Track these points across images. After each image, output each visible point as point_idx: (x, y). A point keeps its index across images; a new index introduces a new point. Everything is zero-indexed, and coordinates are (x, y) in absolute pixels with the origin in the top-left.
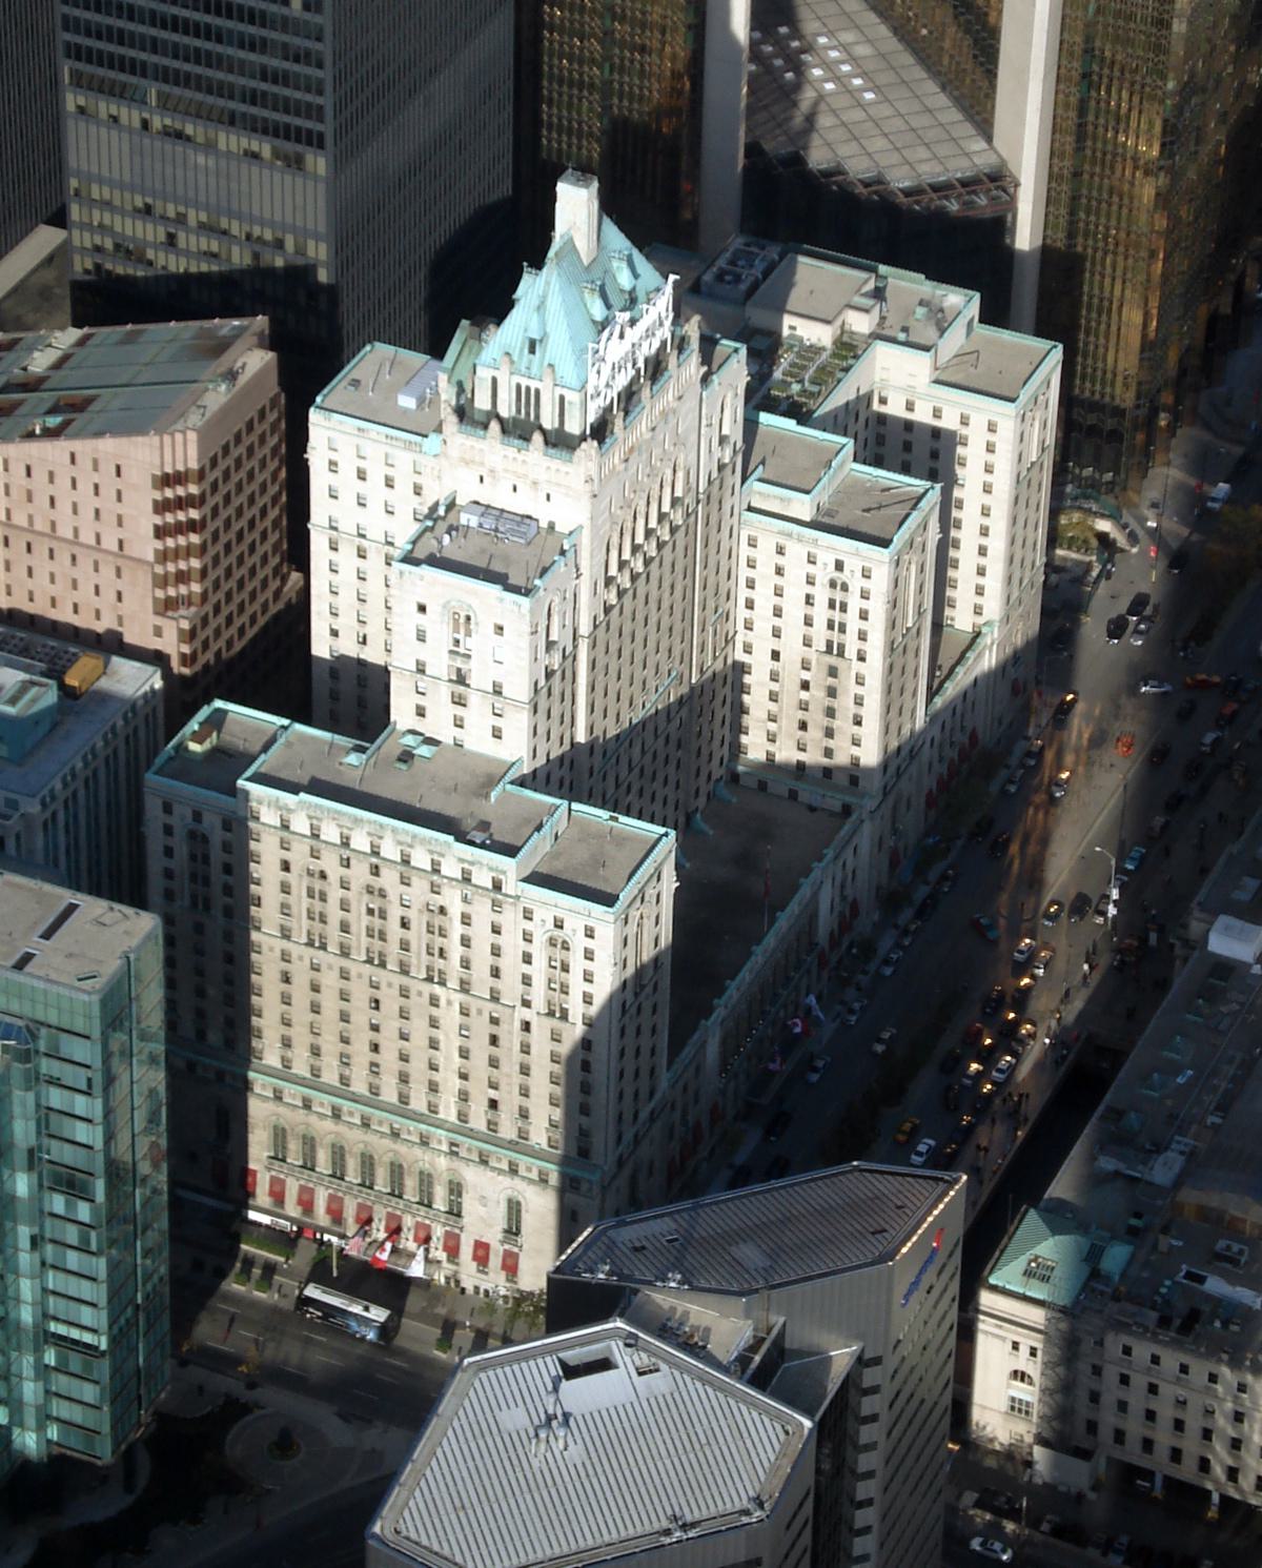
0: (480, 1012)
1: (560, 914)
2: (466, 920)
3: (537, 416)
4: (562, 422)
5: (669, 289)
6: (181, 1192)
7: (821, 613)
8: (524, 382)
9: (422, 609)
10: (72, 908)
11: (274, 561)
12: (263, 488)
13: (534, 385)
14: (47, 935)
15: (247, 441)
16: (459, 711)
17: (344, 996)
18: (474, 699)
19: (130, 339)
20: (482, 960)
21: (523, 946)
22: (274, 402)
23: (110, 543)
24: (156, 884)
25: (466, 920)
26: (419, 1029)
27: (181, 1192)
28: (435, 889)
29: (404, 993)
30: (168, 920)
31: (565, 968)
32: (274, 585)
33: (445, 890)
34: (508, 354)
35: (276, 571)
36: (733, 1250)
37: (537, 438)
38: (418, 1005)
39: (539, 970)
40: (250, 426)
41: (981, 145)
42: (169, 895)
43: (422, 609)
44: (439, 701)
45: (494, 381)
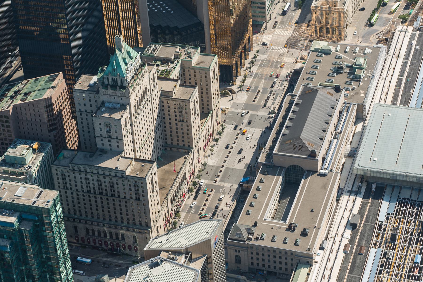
0: (110, 199)
1: (136, 180)
2: (117, 184)
3: (117, 83)
4: (122, 84)
5: (139, 54)
6: (70, 243)
8: (114, 77)
9: (100, 124)
10: (42, 192)
11: (70, 119)
12: (66, 105)
13: (115, 77)
14: (38, 198)
15: (61, 97)
16: (110, 143)
17: (102, 202)
19: (36, 80)
20: (73, 184)
21: (80, 180)
22: (65, 88)
23: (38, 120)
24: (56, 185)
25: (69, 176)
26: (111, 206)
27: (70, 243)
28: (86, 175)
29: (95, 198)
30: (60, 192)
31: (138, 190)
32: (70, 124)
33: (112, 179)
34: (240, 161)
35: (70, 121)
36: (178, 239)
37: (118, 88)
38: (111, 201)
39: (84, 185)
40: (62, 94)
41: (196, 19)
42: (59, 187)
44: (106, 141)
45: (108, 78)
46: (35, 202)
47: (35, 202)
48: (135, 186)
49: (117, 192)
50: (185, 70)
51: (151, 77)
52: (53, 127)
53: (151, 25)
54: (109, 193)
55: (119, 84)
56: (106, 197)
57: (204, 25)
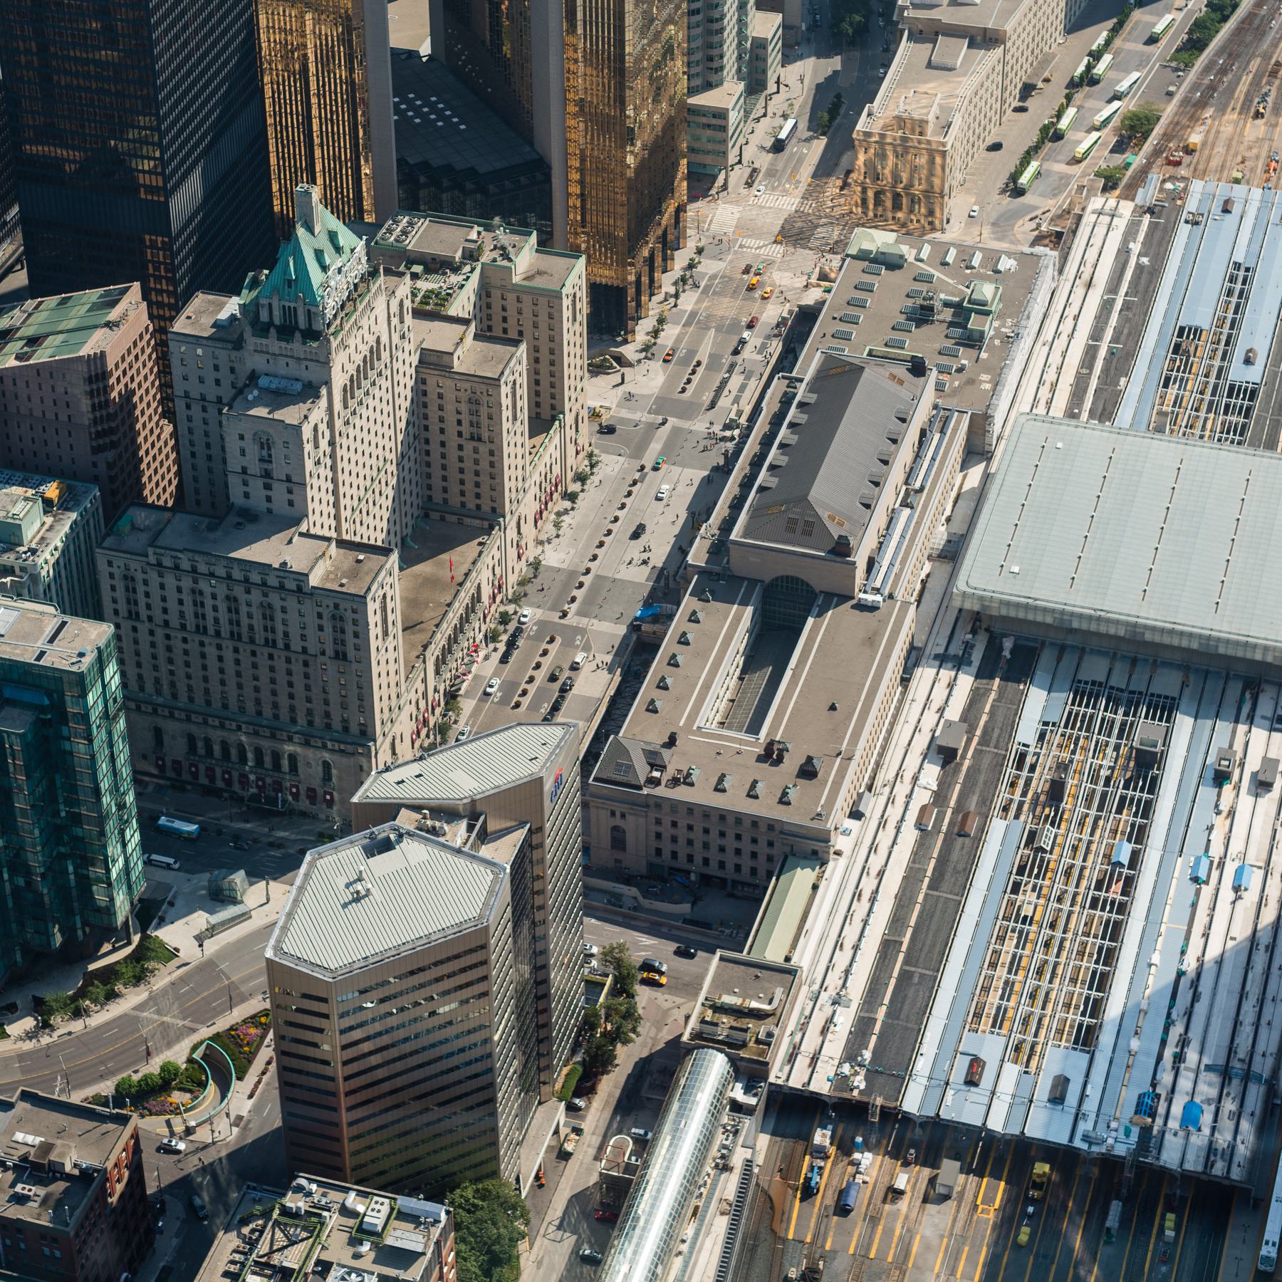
7: (465, 418)
9: (242, 437)
18: (275, 485)
43: (242, 437)
46: (42, 654)
47: (42, 654)
48: (334, 617)
49: (281, 635)
50: (493, 292)
51: (394, 308)
52: (107, 440)
53: (401, 162)
54: (260, 636)
55: (302, 323)
56: (249, 648)
57: (550, 168)
